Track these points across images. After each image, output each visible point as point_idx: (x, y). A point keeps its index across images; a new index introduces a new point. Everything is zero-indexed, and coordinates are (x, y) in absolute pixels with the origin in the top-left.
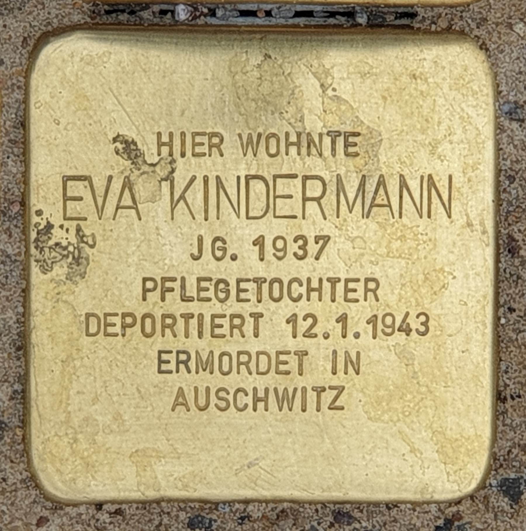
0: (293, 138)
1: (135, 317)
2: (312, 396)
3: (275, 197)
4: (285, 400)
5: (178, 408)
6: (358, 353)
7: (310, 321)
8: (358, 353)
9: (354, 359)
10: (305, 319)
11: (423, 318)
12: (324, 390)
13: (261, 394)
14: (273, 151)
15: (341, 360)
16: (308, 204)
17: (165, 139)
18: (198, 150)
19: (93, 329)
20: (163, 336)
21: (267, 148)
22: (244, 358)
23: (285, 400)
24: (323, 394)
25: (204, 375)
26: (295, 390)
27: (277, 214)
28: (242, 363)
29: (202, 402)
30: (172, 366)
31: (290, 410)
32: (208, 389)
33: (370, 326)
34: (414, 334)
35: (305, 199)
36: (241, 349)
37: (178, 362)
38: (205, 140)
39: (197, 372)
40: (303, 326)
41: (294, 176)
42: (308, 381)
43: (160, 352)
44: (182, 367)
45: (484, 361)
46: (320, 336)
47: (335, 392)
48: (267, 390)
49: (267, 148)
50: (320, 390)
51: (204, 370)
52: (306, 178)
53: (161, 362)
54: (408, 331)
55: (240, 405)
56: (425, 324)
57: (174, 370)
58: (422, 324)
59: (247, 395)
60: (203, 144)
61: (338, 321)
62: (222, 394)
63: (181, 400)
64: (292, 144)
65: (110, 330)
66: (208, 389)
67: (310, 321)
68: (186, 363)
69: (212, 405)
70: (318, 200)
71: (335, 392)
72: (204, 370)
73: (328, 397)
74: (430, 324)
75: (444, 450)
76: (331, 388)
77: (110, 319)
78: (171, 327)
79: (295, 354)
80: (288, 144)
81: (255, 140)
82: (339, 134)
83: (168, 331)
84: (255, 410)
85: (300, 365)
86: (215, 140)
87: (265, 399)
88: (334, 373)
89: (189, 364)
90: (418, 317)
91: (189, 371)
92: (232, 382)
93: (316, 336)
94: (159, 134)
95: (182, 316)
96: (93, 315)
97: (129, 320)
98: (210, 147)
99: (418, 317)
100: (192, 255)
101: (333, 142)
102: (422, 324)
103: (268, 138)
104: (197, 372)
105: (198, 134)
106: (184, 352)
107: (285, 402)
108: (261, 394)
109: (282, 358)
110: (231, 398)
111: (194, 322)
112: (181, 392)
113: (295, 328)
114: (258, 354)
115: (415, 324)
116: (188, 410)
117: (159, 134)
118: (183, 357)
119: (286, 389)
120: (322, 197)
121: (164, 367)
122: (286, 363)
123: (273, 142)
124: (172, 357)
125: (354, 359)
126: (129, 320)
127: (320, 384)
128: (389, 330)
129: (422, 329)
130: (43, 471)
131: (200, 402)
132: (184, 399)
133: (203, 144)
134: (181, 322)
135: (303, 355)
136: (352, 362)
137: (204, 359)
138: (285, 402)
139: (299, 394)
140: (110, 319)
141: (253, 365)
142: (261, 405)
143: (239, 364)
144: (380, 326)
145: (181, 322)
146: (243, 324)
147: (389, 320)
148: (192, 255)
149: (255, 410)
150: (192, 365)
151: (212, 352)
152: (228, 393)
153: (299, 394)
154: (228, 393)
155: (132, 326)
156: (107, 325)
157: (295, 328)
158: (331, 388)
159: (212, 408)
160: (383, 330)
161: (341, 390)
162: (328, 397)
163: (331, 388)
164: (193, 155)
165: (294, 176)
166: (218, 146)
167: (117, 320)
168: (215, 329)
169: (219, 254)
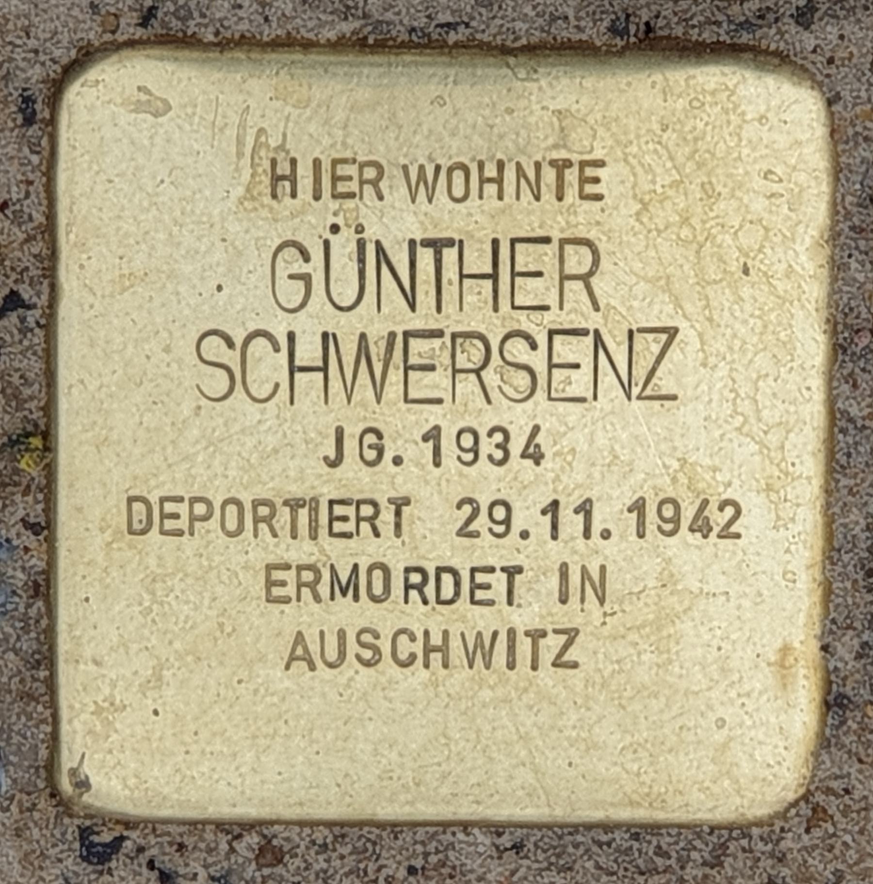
0: (491, 171)
2: (524, 646)
5: (295, 664)
6: (603, 568)
7: (729, 511)
8: (603, 568)
9: (596, 576)
12: (544, 634)
13: (436, 640)
15: (575, 578)
16: (568, 284)
17: (284, 168)
18: (342, 187)
20: (256, 536)
24: (542, 642)
26: (495, 634)
27: (517, 303)
28: (413, 587)
29: (332, 654)
30: (290, 590)
33: (581, 517)
35: (564, 278)
37: (299, 586)
39: (332, 598)
41: (547, 240)
42: (522, 618)
43: (269, 568)
44: (306, 592)
51: (344, 593)
52: (454, 336)
53: (270, 584)
55: (403, 656)
57: (294, 596)
60: (350, 178)
64: (490, 180)
66: (342, 635)
67: (729, 511)
68: (313, 586)
70: (585, 279)
71: (563, 638)
73: (552, 643)
75: (747, 743)
76: (556, 631)
78: (268, 520)
79: (503, 569)
80: (483, 181)
82: (568, 164)
83: (263, 527)
85: (510, 592)
89: (319, 587)
97: (200, 509)
98: (362, 183)
100: (326, 458)
101: (560, 178)
103: (450, 170)
104: (332, 598)
106: (309, 567)
108: (436, 640)
109: (480, 578)
110: (386, 648)
111: (303, 514)
112: (299, 638)
114: (440, 570)
119: (479, 634)
120: (591, 273)
121: (276, 591)
123: (458, 177)
124: (289, 576)
125: (596, 576)
126: (200, 509)
127: (537, 624)
130: (159, 806)
131: (236, 514)
132: (306, 649)
133: (350, 178)
137: (344, 578)
141: (430, 590)
142: (436, 658)
145: (285, 514)
146: (273, 515)
148: (326, 458)
150: (324, 589)
151: (356, 567)
155: (206, 518)
156: (163, 516)
161: (571, 635)
162: (552, 643)
164: (334, 196)
165: (547, 240)
166: (375, 183)
167: (183, 509)
168: (166, 521)
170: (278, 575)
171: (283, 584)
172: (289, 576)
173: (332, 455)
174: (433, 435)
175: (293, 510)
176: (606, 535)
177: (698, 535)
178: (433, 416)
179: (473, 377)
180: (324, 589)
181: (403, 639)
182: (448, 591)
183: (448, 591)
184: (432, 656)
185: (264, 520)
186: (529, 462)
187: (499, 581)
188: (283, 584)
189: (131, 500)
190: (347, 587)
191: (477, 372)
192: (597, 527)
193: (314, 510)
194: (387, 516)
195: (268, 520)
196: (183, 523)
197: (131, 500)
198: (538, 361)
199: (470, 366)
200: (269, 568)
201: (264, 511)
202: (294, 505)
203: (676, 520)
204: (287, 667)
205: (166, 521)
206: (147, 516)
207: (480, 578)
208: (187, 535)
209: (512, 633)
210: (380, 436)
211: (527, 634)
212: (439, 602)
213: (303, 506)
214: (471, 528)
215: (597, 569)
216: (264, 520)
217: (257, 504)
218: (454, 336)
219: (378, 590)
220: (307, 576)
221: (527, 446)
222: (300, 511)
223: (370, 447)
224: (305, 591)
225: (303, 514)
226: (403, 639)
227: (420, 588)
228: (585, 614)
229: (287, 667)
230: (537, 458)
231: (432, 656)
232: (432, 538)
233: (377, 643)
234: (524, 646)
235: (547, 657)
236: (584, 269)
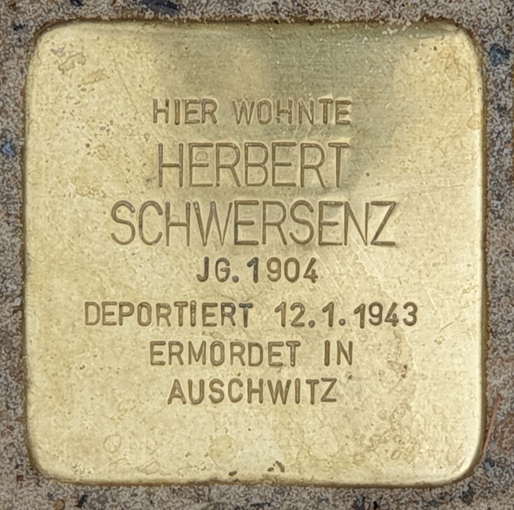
1: (132, 306)
2: (305, 389)
3: (191, 166)
4: (280, 392)
5: (175, 400)
6: (351, 344)
7: (298, 310)
8: (351, 344)
10: (293, 308)
11: (410, 309)
12: (317, 382)
13: (255, 385)
14: (265, 119)
19: (92, 319)
21: (259, 116)
22: (237, 349)
23: (280, 392)
25: (197, 365)
29: (196, 396)
30: (165, 358)
31: (284, 403)
32: (202, 383)
33: (279, 314)
34: (401, 324)
36: (273, 340)
37: (171, 354)
38: (199, 108)
39: (190, 363)
40: (291, 315)
41: (257, 203)
42: (302, 372)
44: (175, 358)
45: (359, 356)
46: (307, 324)
47: (329, 384)
48: (261, 382)
49: (259, 116)
50: (313, 383)
51: (197, 361)
53: (153, 354)
54: (395, 322)
55: (235, 395)
56: (413, 314)
58: (410, 314)
59: (241, 385)
61: (356, 312)
62: (217, 386)
63: (177, 392)
65: (108, 319)
66: (202, 383)
67: (298, 310)
69: (206, 396)
70: (231, 168)
72: (197, 361)
74: (417, 314)
75: (447, 443)
77: (108, 309)
81: (248, 108)
84: (250, 401)
86: (209, 107)
87: (260, 391)
88: (327, 364)
90: (405, 307)
91: (182, 363)
92: (225, 373)
93: (303, 325)
94: (155, 103)
95: (176, 304)
96: (93, 304)
99: (405, 307)
102: (410, 314)
104: (190, 363)
105: (191, 102)
107: (279, 395)
109: (275, 349)
110: (225, 389)
113: (362, 318)
115: (402, 314)
116: (184, 403)
117: (155, 103)
118: (176, 349)
121: (157, 358)
122: (279, 354)
124: (165, 349)
128: (375, 320)
129: (410, 319)
134: (239, 312)
135: (296, 346)
136: (195, 356)
138: (279, 395)
139: (292, 387)
140: (109, 309)
141: (245, 357)
142: (255, 396)
143: (233, 355)
144: (367, 316)
145: (175, 310)
147: (376, 310)
149: (250, 401)
150: (185, 356)
152: (222, 385)
153: (292, 387)
154: (222, 385)
156: (105, 314)
157: (362, 318)
158: (324, 380)
159: (207, 400)
160: (370, 321)
163: (324, 380)
168: (106, 317)
169: (222, 275)
170: (157, 348)
171: (161, 353)
172: (165, 349)
173: (202, 275)
174: (254, 263)
175: (181, 309)
176: (342, 323)
177: (391, 324)
178: (252, 253)
179: (276, 228)
180: (185, 356)
181: (235, 386)
182: (256, 358)
183: (256, 358)
184: (253, 395)
185: (163, 316)
186: (309, 281)
187: (286, 351)
188: (161, 353)
189: (87, 304)
190: (198, 355)
191: (278, 225)
192: (336, 322)
193: (193, 309)
194: (239, 312)
195: (166, 316)
196: (115, 318)
197: (87, 304)
198: (314, 219)
199: (275, 221)
200: (153, 344)
201: (163, 311)
202: (181, 305)
203: (380, 316)
204: (170, 402)
205: (106, 317)
206: (102, 313)
207: (275, 349)
208: (118, 325)
209: (298, 380)
210: (228, 264)
211: (308, 382)
212: (251, 365)
213: (186, 305)
214: (300, 321)
215: (348, 344)
216: (163, 316)
217: (159, 306)
218: (265, 203)
219: (217, 358)
220: (176, 349)
221: (308, 271)
222: (184, 308)
223: (222, 270)
224: (174, 358)
225: (187, 311)
226: (235, 386)
227: (240, 355)
228: (339, 370)
229: (170, 402)
230: (313, 278)
231: (253, 395)
232: (264, 325)
233: (222, 388)
234: (305, 389)
235: (318, 396)
236: (231, 162)
